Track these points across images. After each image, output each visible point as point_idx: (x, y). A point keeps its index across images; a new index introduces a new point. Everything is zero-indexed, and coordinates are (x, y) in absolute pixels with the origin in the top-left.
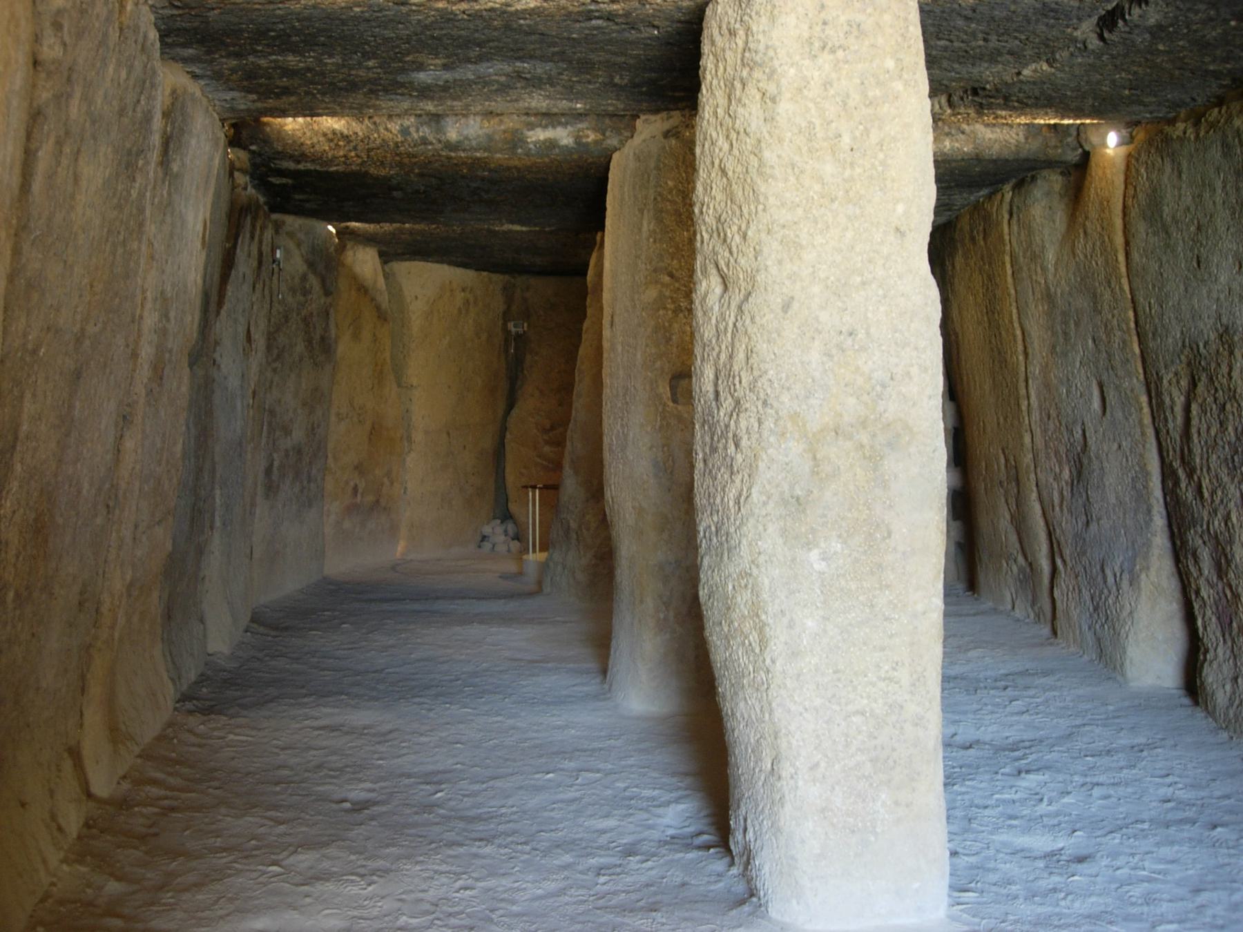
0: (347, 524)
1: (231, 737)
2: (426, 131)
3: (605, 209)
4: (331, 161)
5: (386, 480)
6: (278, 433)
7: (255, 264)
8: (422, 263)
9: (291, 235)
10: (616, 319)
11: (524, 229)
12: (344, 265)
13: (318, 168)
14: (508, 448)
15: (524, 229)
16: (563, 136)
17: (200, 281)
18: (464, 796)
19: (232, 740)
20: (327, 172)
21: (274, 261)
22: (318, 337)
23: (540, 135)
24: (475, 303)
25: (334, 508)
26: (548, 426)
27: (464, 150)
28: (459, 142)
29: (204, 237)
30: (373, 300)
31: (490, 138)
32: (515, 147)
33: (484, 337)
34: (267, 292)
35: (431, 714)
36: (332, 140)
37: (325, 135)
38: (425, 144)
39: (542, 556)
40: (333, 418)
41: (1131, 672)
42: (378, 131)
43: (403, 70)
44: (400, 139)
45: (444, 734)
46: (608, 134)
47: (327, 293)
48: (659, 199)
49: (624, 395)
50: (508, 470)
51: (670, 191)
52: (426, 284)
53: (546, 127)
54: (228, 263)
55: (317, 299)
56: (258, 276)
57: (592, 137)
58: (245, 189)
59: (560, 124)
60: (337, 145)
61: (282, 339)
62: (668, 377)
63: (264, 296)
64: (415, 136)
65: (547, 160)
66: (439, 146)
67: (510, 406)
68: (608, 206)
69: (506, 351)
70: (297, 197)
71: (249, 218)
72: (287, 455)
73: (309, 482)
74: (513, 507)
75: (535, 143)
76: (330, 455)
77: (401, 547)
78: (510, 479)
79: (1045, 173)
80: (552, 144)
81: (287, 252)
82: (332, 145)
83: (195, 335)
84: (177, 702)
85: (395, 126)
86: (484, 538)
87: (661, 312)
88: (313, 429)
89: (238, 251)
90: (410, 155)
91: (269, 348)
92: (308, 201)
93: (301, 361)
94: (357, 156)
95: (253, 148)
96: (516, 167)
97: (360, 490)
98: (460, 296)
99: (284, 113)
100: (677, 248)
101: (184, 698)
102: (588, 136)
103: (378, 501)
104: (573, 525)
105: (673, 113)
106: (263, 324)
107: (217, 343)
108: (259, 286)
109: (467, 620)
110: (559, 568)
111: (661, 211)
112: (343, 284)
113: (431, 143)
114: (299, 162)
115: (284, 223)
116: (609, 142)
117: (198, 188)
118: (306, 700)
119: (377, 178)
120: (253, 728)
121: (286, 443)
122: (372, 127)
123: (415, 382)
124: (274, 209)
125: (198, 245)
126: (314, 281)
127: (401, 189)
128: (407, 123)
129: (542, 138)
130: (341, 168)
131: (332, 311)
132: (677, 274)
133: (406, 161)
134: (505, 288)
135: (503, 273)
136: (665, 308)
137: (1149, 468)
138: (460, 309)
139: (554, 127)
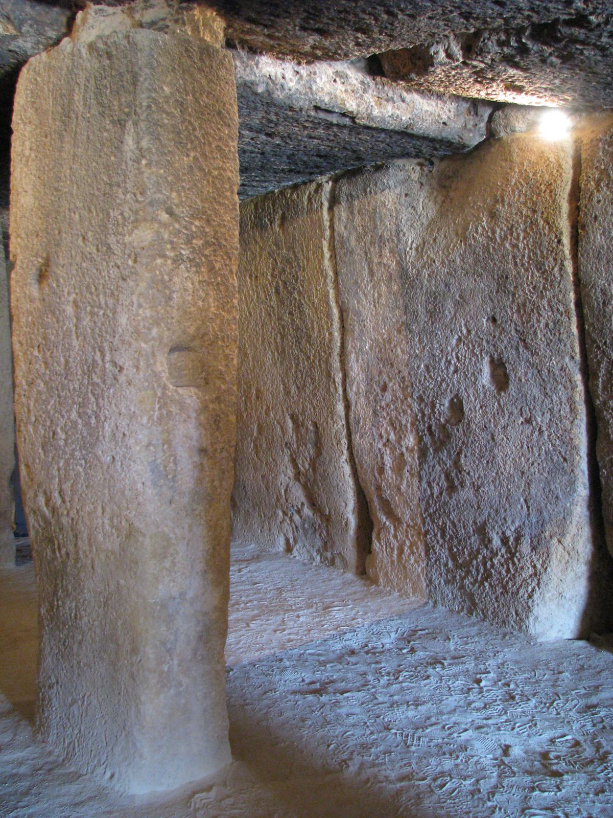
3: (10, 132)
41: (534, 628)
46: (25, 29)
48: (154, 107)
62: (167, 350)
79: (400, 162)
100: (177, 178)
132: (177, 211)
136: (164, 256)
137: (576, 442)
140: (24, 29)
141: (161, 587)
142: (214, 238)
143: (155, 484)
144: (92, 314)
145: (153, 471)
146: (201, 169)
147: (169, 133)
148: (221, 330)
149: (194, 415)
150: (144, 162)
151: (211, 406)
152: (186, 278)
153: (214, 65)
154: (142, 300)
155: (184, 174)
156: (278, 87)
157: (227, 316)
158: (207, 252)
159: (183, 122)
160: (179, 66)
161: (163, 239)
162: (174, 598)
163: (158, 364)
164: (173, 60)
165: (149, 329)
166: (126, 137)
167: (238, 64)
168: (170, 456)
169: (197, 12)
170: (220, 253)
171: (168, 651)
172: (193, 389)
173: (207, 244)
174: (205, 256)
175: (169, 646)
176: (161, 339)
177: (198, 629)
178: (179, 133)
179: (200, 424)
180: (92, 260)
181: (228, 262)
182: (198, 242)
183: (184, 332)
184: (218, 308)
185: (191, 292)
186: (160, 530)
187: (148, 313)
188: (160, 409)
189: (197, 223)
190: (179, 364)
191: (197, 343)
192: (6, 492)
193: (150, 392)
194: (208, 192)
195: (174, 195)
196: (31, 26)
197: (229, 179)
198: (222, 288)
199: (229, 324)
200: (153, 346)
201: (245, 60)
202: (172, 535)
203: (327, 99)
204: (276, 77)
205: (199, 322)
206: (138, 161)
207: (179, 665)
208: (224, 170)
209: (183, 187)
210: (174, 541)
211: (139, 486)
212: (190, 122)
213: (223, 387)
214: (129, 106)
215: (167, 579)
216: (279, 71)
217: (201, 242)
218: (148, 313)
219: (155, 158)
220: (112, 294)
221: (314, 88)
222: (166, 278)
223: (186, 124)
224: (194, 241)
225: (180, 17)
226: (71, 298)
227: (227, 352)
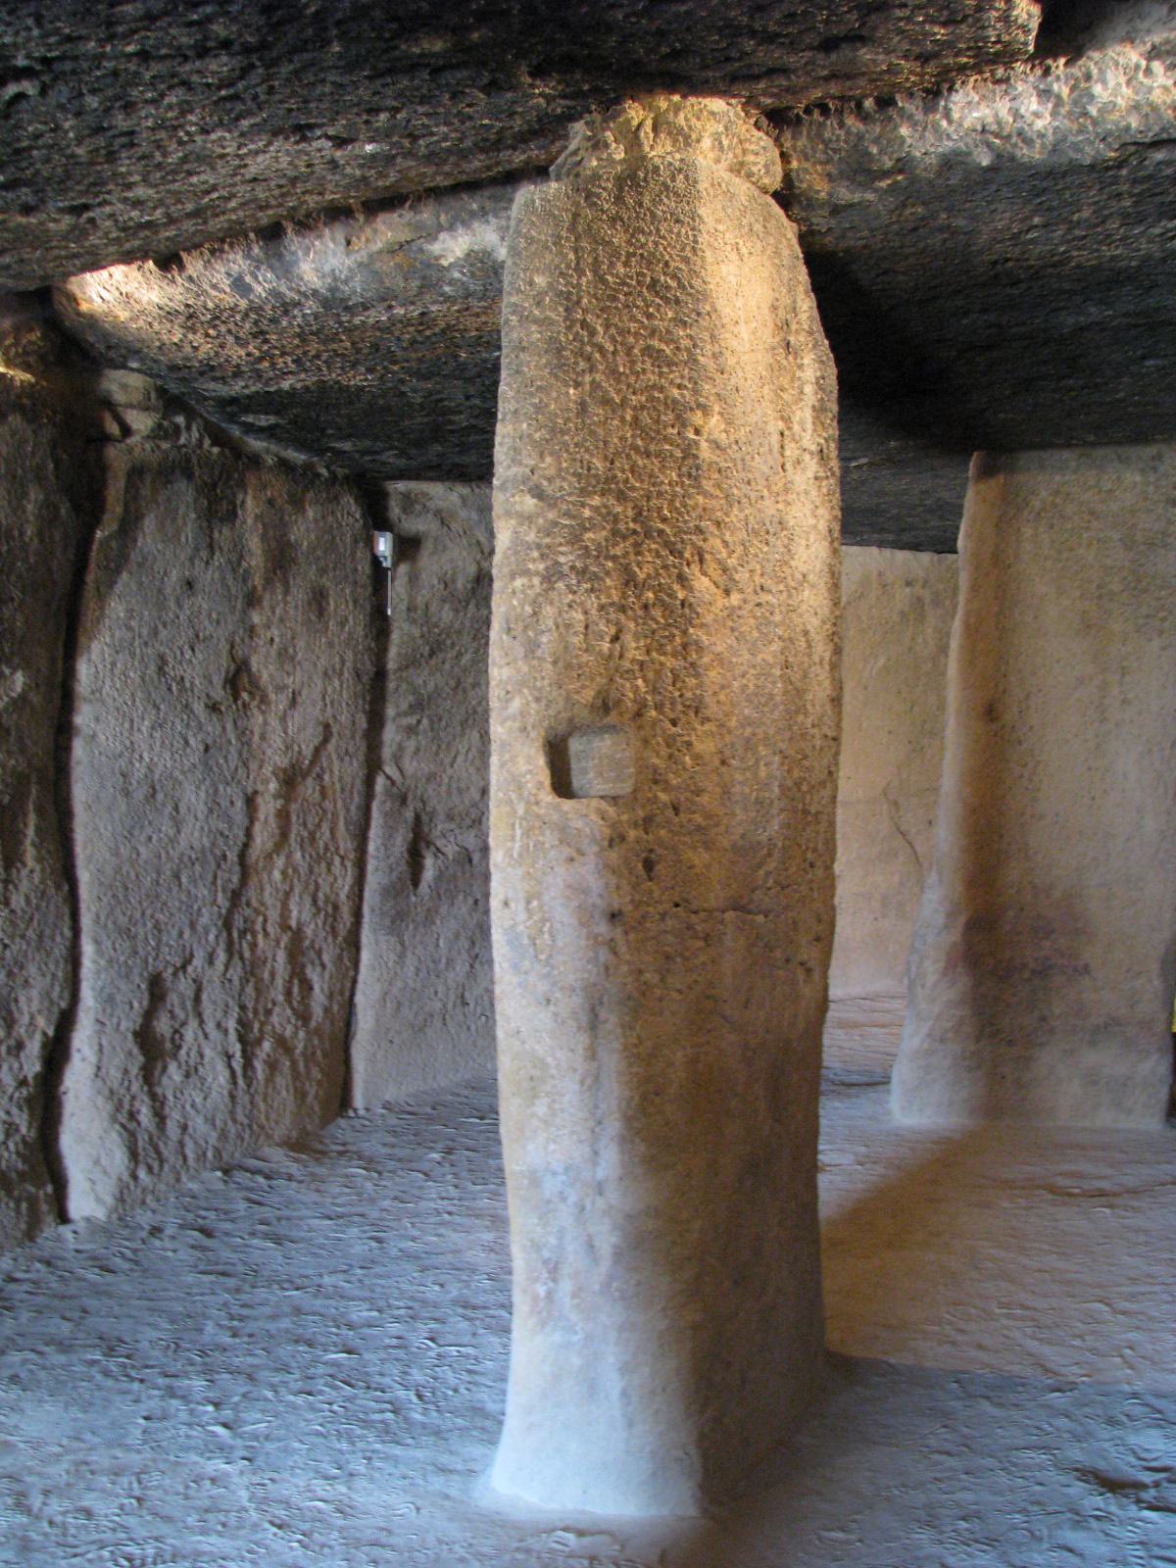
136: (526, 573)
142: (634, 521)
146: (606, 402)
147: (539, 355)
151: (632, 834)
152: (570, 606)
153: (646, 201)
156: (1014, 139)
157: (670, 662)
158: (618, 551)
159: (569, 328)
162: (554, 1173)
163: (521, 760)
168: (544, 921)
169: (635, 112)
174: (614, 558)
178: (559, 351)
179: (607, 866)
186: (527, 1047)
190: (618, 756)
192: (1156, 982)
197: (675, 401)
201: (919, 116)
202: (550, 1060)
203: (1134, 122)
204: (999, 123)
207: (574, 1296)
209: (565, 444)
210: (553, 1071)
213: (663, 797)
216: (1003, 108)
217: (604, 533)
221: (1093, 111)
224: (589, 535)
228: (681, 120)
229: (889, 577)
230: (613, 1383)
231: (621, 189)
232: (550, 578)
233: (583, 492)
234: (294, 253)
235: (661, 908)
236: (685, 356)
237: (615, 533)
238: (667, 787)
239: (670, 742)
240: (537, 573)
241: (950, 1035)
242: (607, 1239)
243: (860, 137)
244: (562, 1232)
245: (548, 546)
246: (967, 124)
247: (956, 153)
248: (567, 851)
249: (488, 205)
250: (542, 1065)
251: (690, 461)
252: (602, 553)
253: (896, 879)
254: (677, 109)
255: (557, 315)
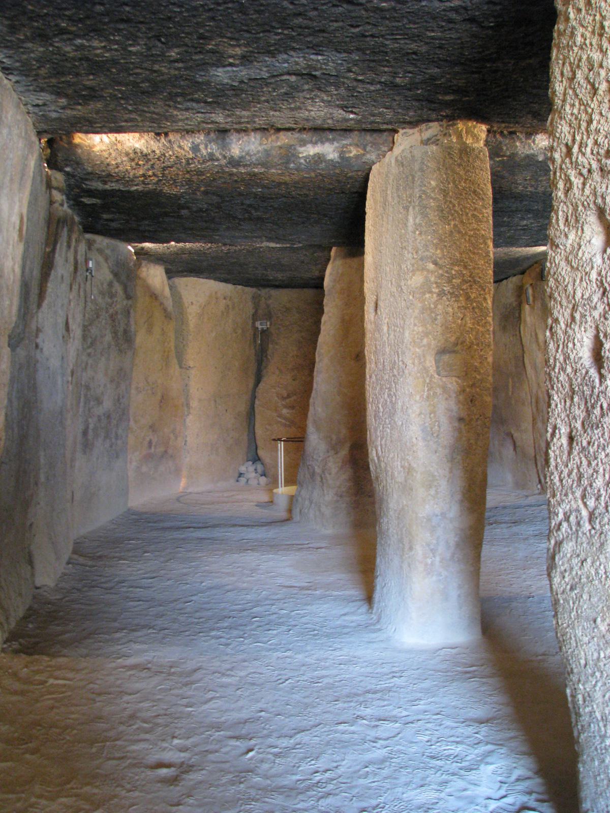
0: (144, 469)
1: (51, 681)
2: (214, 148)
3: (365, 213)
4: (132, 181)
5: (172, 435)
6: (92, 403)
7: (72, 269)
8: (195, 279)
9: (100, 251)
10: (381, 304)
11: (278, 246)
12: (140, 278)
13: (122, 188)
14: (257, 411)
15: (278, 246)
16: (329, 150)
17: (18, 270)
18: (276, 755)
19: (52, 684)
20: (129, 192)
21: (87, 270)
22: (122, 329)
23: (311, 150)
24: (233, 308)
25: (134, 458)
26: (285, 395)
27: (245, 166)
28: (241, 157)
29: (20, 230)
30: (161, 304)
31: (267, 153)
32: (288, 162)
33: (240, 331)
34: (82, 293)
35: (229, 650)
36: (133, 160)
37: (127, 154)
38: (212, 160)
39: (292, 490)
40: (133, 391)
42: (172, 148)
43: (203, 65)
44: (191, 155)
45: (243, 674)
46: (368, 148)
47: (128, 297)
48: (424, 196)
49: (392, 369)
50: (256, 427)
51: (433, 190)
52: (199, 293)
53: (316, 143)
54: (47, 265)
55: (121, 302)
56: (74, 278)
57: (354, 152)
58: (62, 205)
59: (328, 140)
60: (137, 164)
61: (94, 331)
62: (433, 352)
63: (79, 296)
64: (204, 152)
65: (313, 175)
66: (223, 162)
67: (258, 380)
68: (367, 210)
69: (255, 341)
70: (105, 216)
71: (65, 229)
72: (99, 420)
73: (117, 438)
74: (261, 453)
75: (306, 158)
76: (132, 419)
77: (183, 483)
78: (259, 431)
80: (319, 158)
81: (97, 263)
82: (133, 164)
83: (14, 319)
84: (5, 643)
85: (187, 144)
86: (241, 475)
87: (427, 296)
88: (119, 400)
89: (57, 255)
90: (200, 173)
91: (84, 337)
92: (112, 220)
93: (109, 348)
94: (154, 175)
95: (68, 169)
96: (285, 183)
97: (154, 444)
98: (223, 303)
99: (92, 128)
101: (13, 637)
102: (350, 152)
103: (166, 452)
104: (318, 470)
105: (431, 124)
106: (79, 318)
107: (38, 330)
108: (75, 287)
109: (244, 547)
110: (307, 503)
111: (425, 207)
112: (139, 292)
113: (218, 160)
114: (105, 183)
115: (94, 241)
116: (368, 156)
117: (12, 180)
118: (118, 635)
119: (169, 197)
120: (72, 670)
121: (99, 411)
122: (168, 145)
123: (191, 364)
124: (87, 229)
125: (15, 235)
126: (118, 288)
127: (188, 208)
128: (197, 141)
129: (311, 153)
130: (140, 188)
131: (132, 311)
133: (195, 178)
134: (253, 297)
135: (252, 286)
136: (431, 292)
138: (223, 313)
139: (323, 143)
140: (367, 150)
141: (427, 507)
142: (470, 277)
143: (424, 439)
144: (395, 331)
145: (423, 431)
146: (459, 232)
148: (476, 339)
149: (454, 395)
150: (417, 233)
151: (468, 390)
153: (471, 159)
154: (416, 321)
155: (446, 237)
157: (481, 329)
158: (464, 287)
159: (445, 203)
160: (443, 166)
161: (430, 281)
163: (427, 362)
164: (439, 163)
165: (422, 340)
166: (409, 217)
167: (518, 144)
169: (460, 125)
170: (475, 286)
171: (432, 550)
172: (454, 379)
173: (464, 281)
174: (463, 290)
175: (432, 547)
176: (429, 345)
177: (456, 539)
178: (442, 211)
179: (459, 402)
180: (394, 296)
181: (482, 292)
182: (456, 281)
183: (446, 340)
184: (473, 324)
185: (451, 314)
187: (421, 329)
188: (428, 390)
189: (456, 268)
191: (458, 348)
193: (421, 380)
194: (465, 246)
195: (439, 251)
196: (371, 147)
197: (483, 235)
198: (477, 310)
199: (483, 334)
200: (423, 351)
205: (458, 334)
206: (414, 232)
207: (441, 562)
208: (478, 230)
209: (445, 246)
211: (414, 440)
212: (450, 202)
213: (478, 377)
214: (410, 197)
215: (432, 502)
218: (421, 329)
219: (424, 229)
220: (403, 319)
222: (432, 306)
223: (448, 203)
224: (454, 281)
225: (447, 131)
226: (386, 322)
227: (482, 353)
228: (476, 131)
229: (219, 295)
230: (454, 593)
231: (461, 154)
232: (441, 294)
233: (452, 264)
234: (232, 140)
235: (476, 417)
236: (485, 220)
237: (463, 280)
238: (479, 374)
239: (481, 356)
240: (435, 293)
241: (344, 494)
242: (453, 539)
243: (500, 143)
244: (438, 538)
245: (440, 283)
246: (540, 146)
247: (533, 155)
248: (446, 396)
249: (337, 137)
250: (434, 476)
251: (487, 258)
252: (459, 287)
253: (216, 437)
254: (475, 127)
255: (441, 197)
